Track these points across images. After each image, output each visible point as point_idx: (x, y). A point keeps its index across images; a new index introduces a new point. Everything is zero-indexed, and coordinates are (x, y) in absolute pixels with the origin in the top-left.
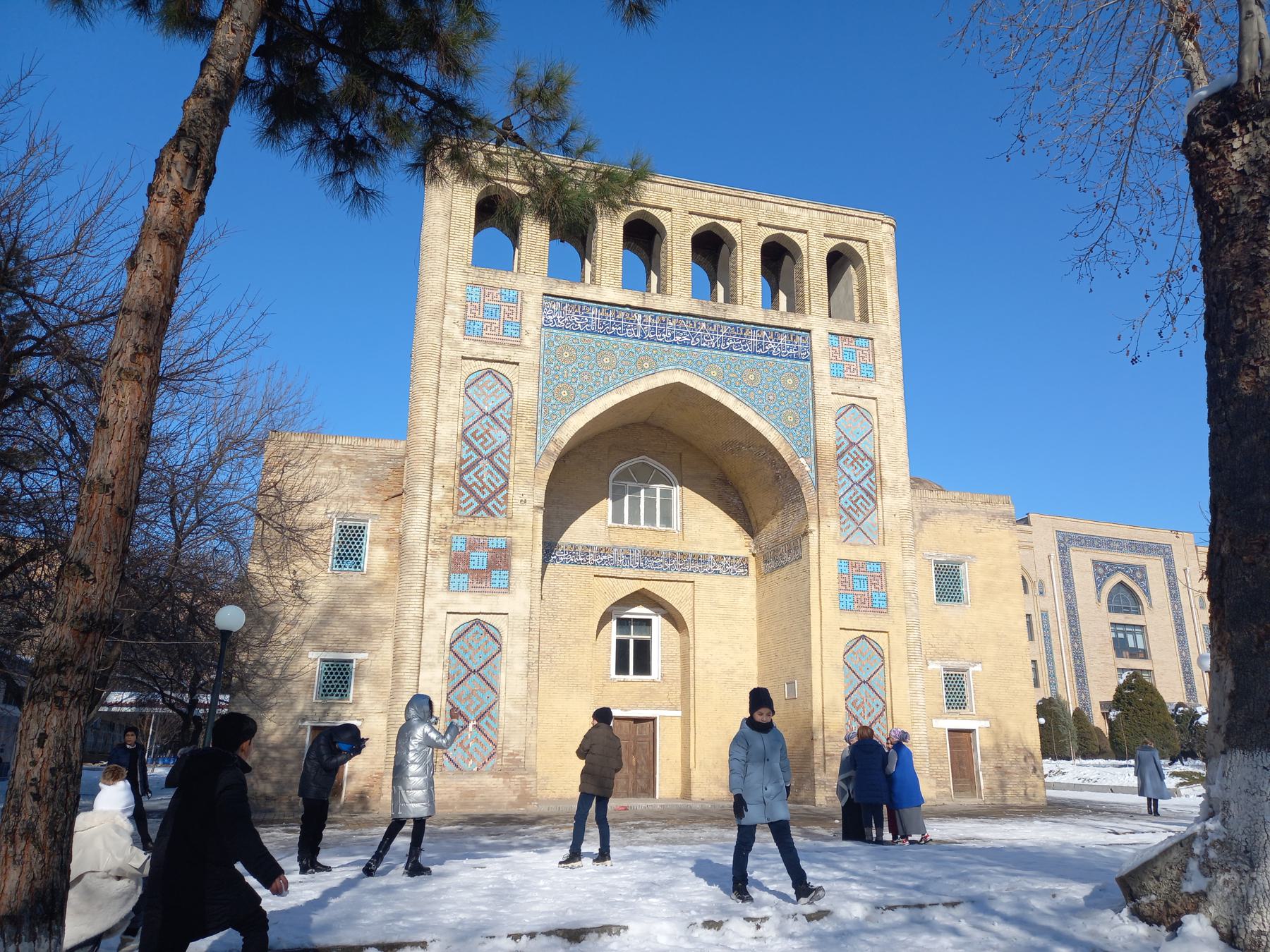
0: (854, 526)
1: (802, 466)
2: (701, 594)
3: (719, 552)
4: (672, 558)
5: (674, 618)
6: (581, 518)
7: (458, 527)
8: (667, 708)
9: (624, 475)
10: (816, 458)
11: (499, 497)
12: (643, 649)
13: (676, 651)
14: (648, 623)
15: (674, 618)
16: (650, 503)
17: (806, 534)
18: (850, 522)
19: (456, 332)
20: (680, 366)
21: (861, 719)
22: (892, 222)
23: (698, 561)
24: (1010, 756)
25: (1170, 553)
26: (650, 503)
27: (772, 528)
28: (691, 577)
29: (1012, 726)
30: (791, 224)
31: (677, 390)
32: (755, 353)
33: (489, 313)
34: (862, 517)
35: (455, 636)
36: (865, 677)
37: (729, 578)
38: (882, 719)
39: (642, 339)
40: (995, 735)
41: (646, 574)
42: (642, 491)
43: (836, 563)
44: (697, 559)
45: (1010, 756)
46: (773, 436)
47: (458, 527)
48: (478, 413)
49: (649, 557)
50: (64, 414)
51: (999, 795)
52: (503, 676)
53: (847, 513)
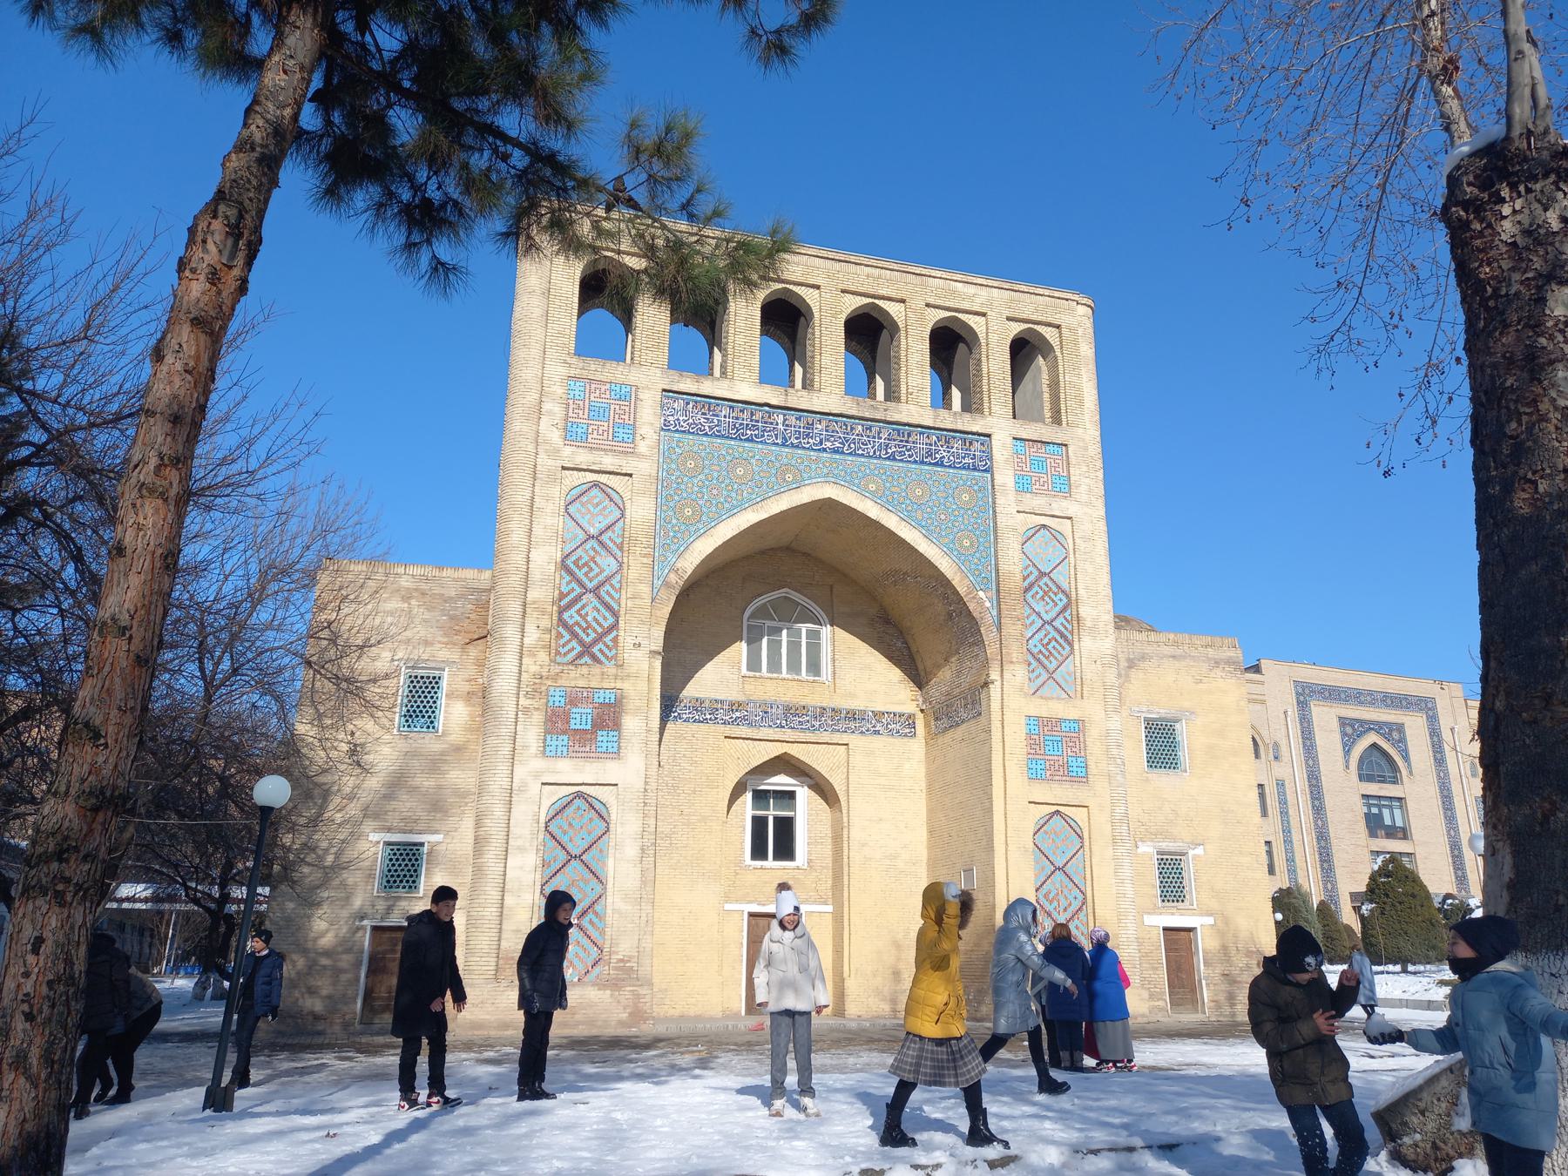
0: (1045, 676)
1: (982, 602)
2: (857, 759)
3: (879, 708)
4: (822, 715)
5: (823, 789)
6: (709, 666)
7: (556, 677)
8: (815, 902)
9: (762, 613)
10: (998, 591)
11: (608, 639)
12: (785, 828)
13: (826, 830)
14: (791, 795)
15: (823, 789)
16: (794, 647)
17: (986, 684)
18: (1040, 670)
19: (555, 436)
20: (831, 478)
21: (1055, 915)
22: (1089, 302)
23: (853, 719)
24: (1240, 961)
25: (1434, 708)
26: (794, 647)
27: (944, 677)
28: (845, 738)
29: (1242, 923)
30: (966, 305)
31: (829, 505)
32: (922, 463)
33: (597, 413)
34: (1055, 663)
35: (552, 813)
36: (1059, 863)
37: (891, 740)
38: (1082, 915)
39: (783, 445)
40: (1222, 934)
41: (789, 734)
42: (785, 632)
43: (1023, 721)
44: (852, 716)
45: (1240, 961)
46: (945, 565)
47: (556, 677)
48: (582, 536)
49: (793, 714)
50: (68, 537)
51: (1227, 1010)
52: (610, 862)
53: (1037, 659)
